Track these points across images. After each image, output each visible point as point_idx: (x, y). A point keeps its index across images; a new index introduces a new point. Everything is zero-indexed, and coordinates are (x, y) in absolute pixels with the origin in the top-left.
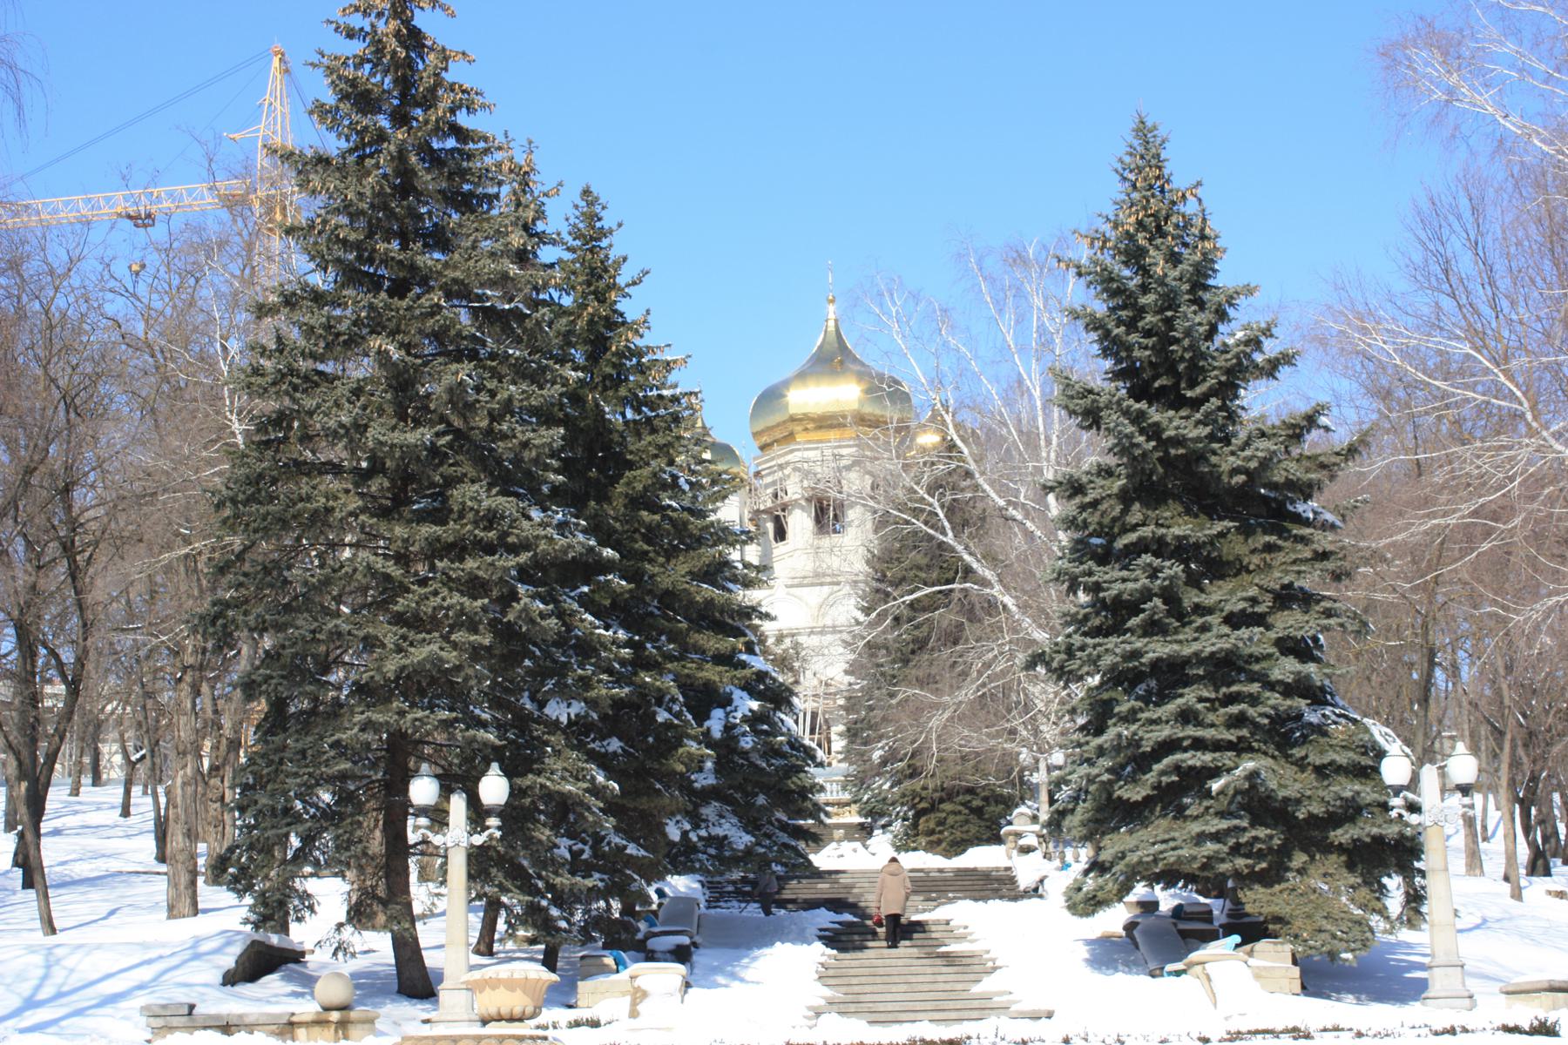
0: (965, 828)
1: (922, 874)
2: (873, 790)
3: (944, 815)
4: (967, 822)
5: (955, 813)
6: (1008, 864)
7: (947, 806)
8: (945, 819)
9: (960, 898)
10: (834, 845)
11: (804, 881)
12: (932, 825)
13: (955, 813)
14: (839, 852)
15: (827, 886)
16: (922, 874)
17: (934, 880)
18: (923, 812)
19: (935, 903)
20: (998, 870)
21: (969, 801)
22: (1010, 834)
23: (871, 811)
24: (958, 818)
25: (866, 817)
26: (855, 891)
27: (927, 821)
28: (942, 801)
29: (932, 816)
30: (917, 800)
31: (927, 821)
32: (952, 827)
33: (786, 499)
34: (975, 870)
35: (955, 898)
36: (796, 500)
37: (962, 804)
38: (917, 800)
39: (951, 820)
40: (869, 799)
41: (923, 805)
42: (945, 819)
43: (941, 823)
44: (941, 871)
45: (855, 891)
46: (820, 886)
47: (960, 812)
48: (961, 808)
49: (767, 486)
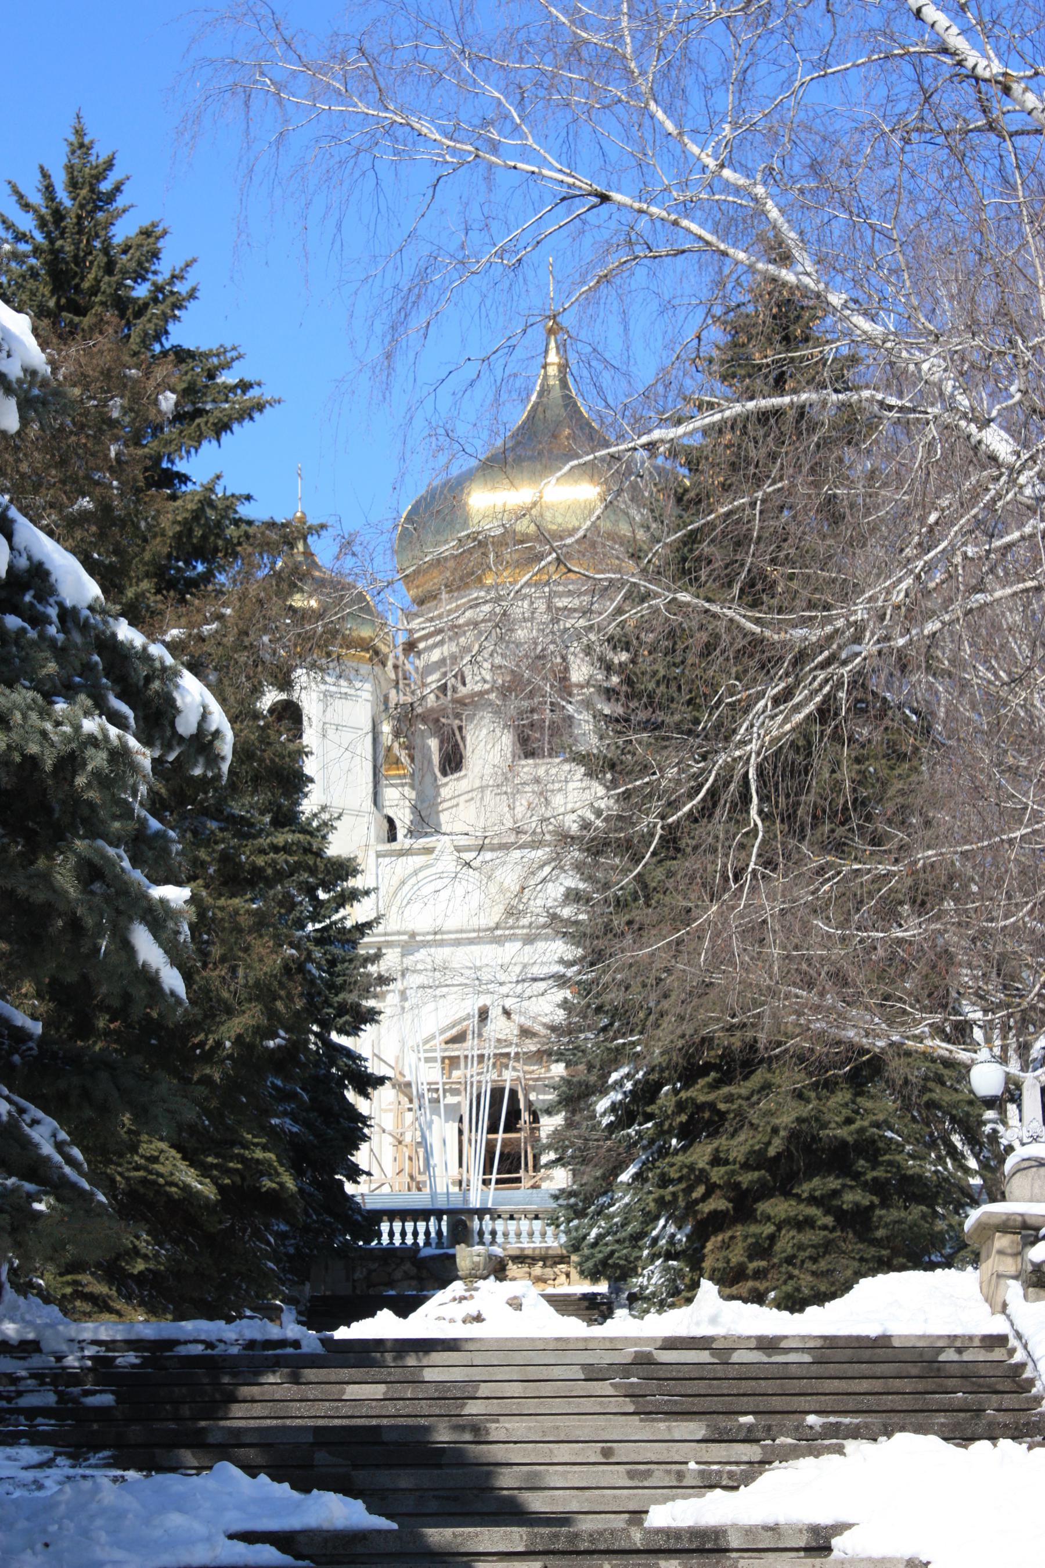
0: (823, 1265)
1: (704, 1356)
2: (610, 1217)
3: (769, 1229)
4: (827, 1247)
5: (804, 1224)
6: (998, 1326)
7: (778, 1207)
8: (772, 1238)
9: (855, 1433)
10: (457, 1287)
11: (310, 1374)
12: (737, 1255)
13: (804, 1224)
14: (470, 1308)
15: (378, 1391)
16: (704, 1356)
17: (748, 1374)
18: (714, 1223)
19: (750, 1452)
20: (959, 1343)
21: (835, 1193)
22: (991, 1228)
23: (604, 1263)
24: (808, 1237)
25: (594, 1276)
26: (473, 1408)
27: (726, 1246)
28: (764, 1192)
29: (739, 1231)
30: (701, 1190)
31: (726, 1246)
32: (789, 1260)
33: (463, 691)
34: (883, 1342)
35: (834, 1431)
36: (481, 694)
37: (812, 1200)
38: (701, 1190)
39: (787, 1241)
40: (600, 1237)
41: (717, 1203)
42: (772, 1238)
43: (761, 1249)
44: (768, 1344)
45: (473, 1408)
46: (352, 1391)
47: (808, 1223)
48: (813, 1211)
49: (429, 669)
